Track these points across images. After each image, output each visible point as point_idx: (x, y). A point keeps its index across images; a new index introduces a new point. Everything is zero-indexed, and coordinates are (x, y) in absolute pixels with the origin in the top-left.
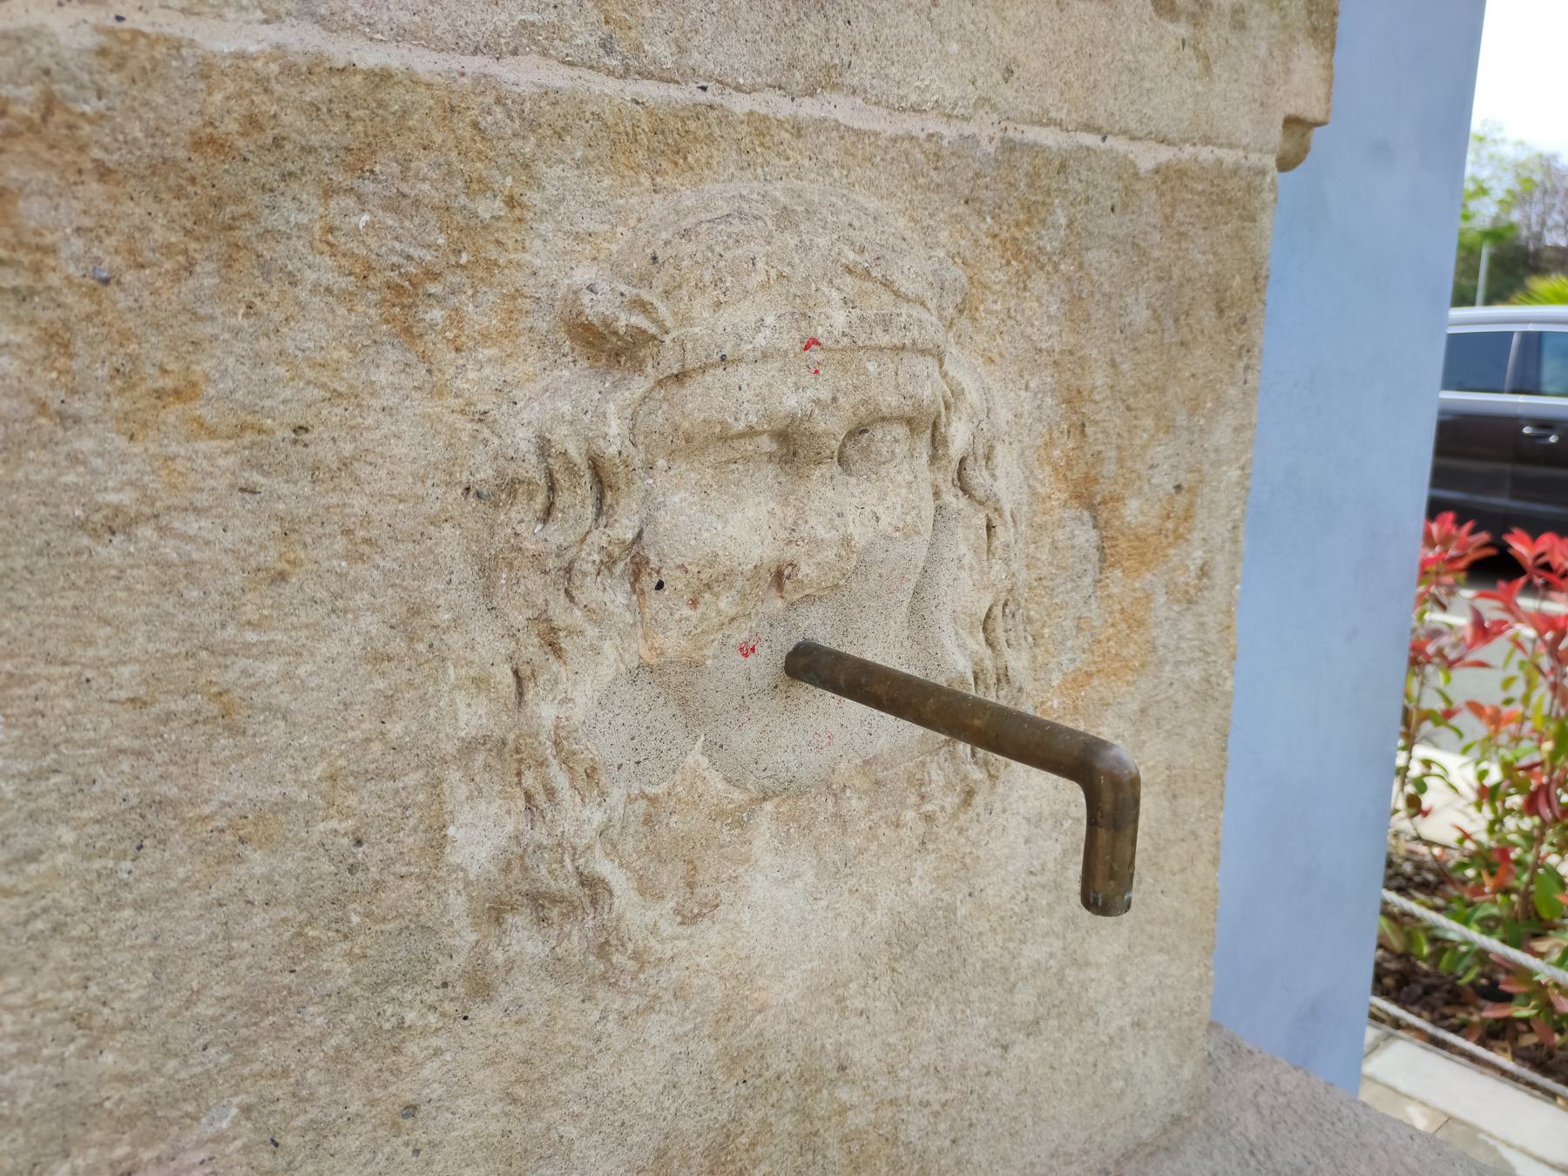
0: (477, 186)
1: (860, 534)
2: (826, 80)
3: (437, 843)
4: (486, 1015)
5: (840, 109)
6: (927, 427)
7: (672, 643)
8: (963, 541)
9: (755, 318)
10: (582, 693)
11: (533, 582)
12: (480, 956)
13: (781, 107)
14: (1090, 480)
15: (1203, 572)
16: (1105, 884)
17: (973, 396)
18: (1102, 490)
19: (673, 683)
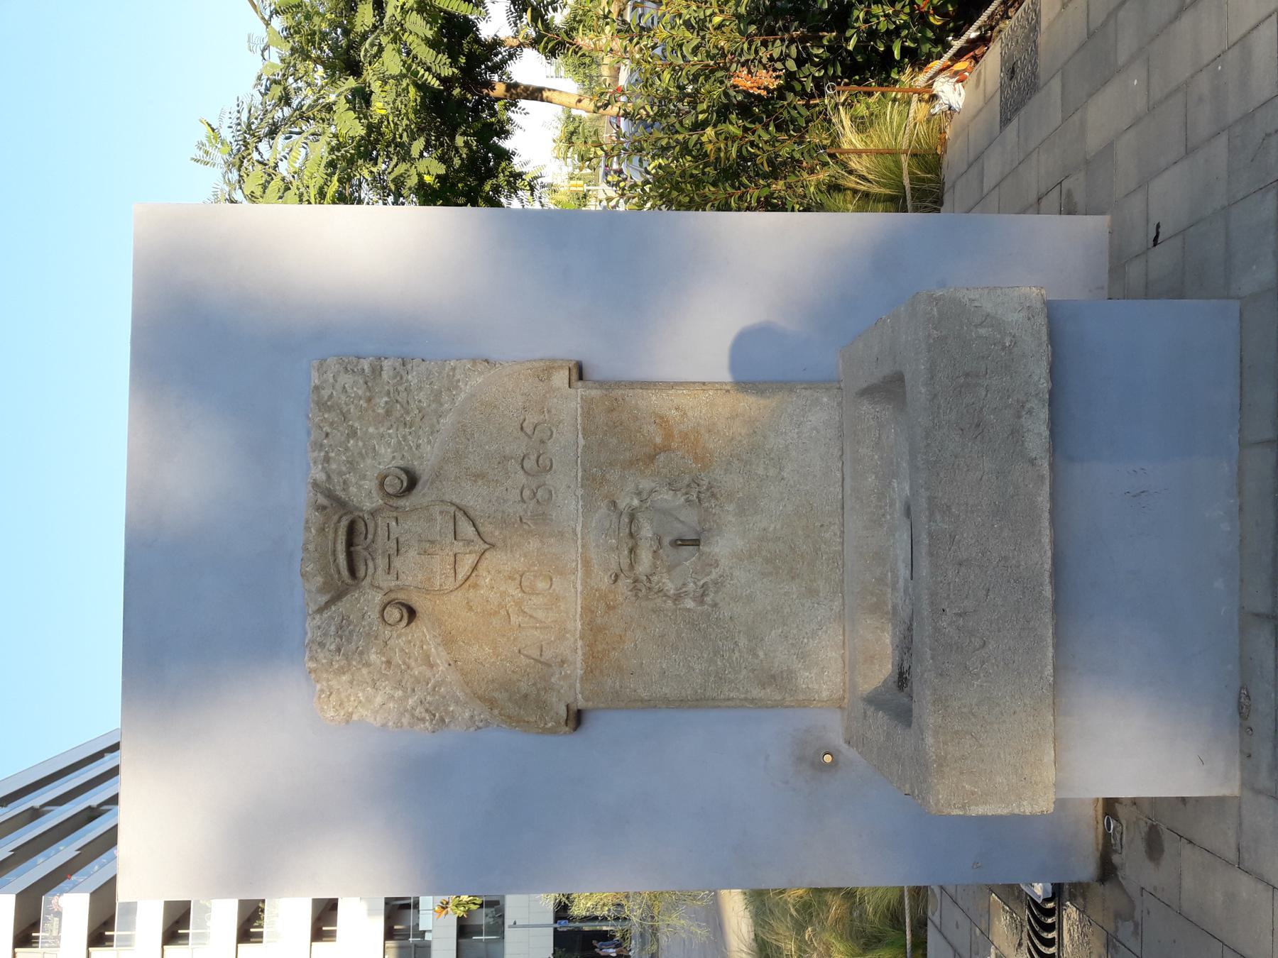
5: (579, 529)
10: (670, 588)
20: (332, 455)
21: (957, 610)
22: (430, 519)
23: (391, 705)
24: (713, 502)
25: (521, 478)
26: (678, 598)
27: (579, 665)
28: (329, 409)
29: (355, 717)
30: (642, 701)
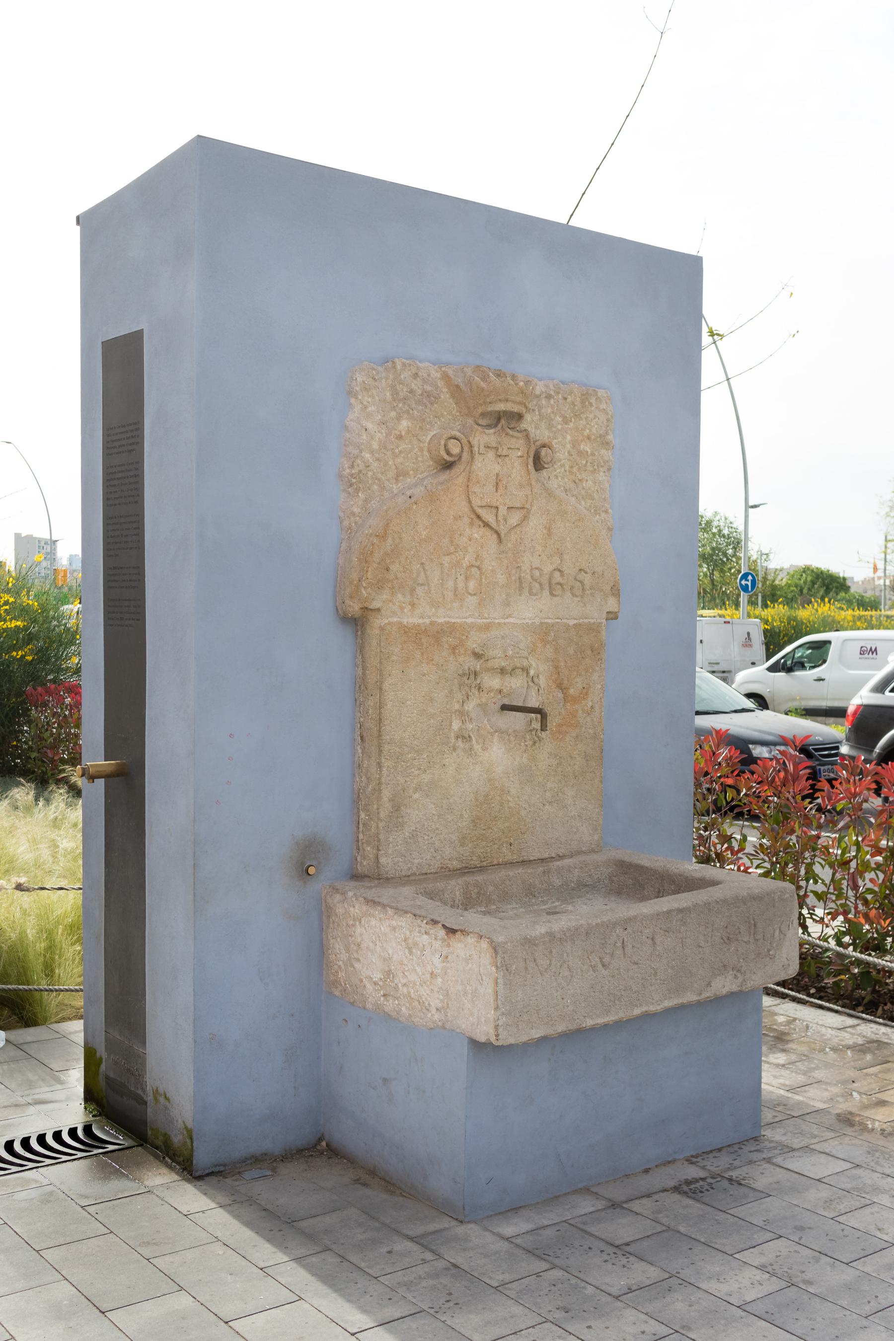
0: (463, 635)
1: (514, 687)
2: (509, 616)
3: (451, 725)
4: (454, 754)
5: (511, 620)
6: (526, 670)
7: (484, 700)
8: (533, 692)
9: (498, 653)
10: (470, 706)
11: (466, 688)
12: (455, 744)
13: (502, 621)
14: (561, 684)
15: (592, 707)
16: (544, 728)
17: (534, 665)
18: (564, 686)
19: (483, 707)
20: (552, 402)
21: (626, 940)
22: (521, 486)
23: (365, 437)
24: (530, 743)
25: (548, 569)
26: (462, 713)
27: (411, 620)
28: (583, 402)
29: (353, 400)
30: (382, 683)
